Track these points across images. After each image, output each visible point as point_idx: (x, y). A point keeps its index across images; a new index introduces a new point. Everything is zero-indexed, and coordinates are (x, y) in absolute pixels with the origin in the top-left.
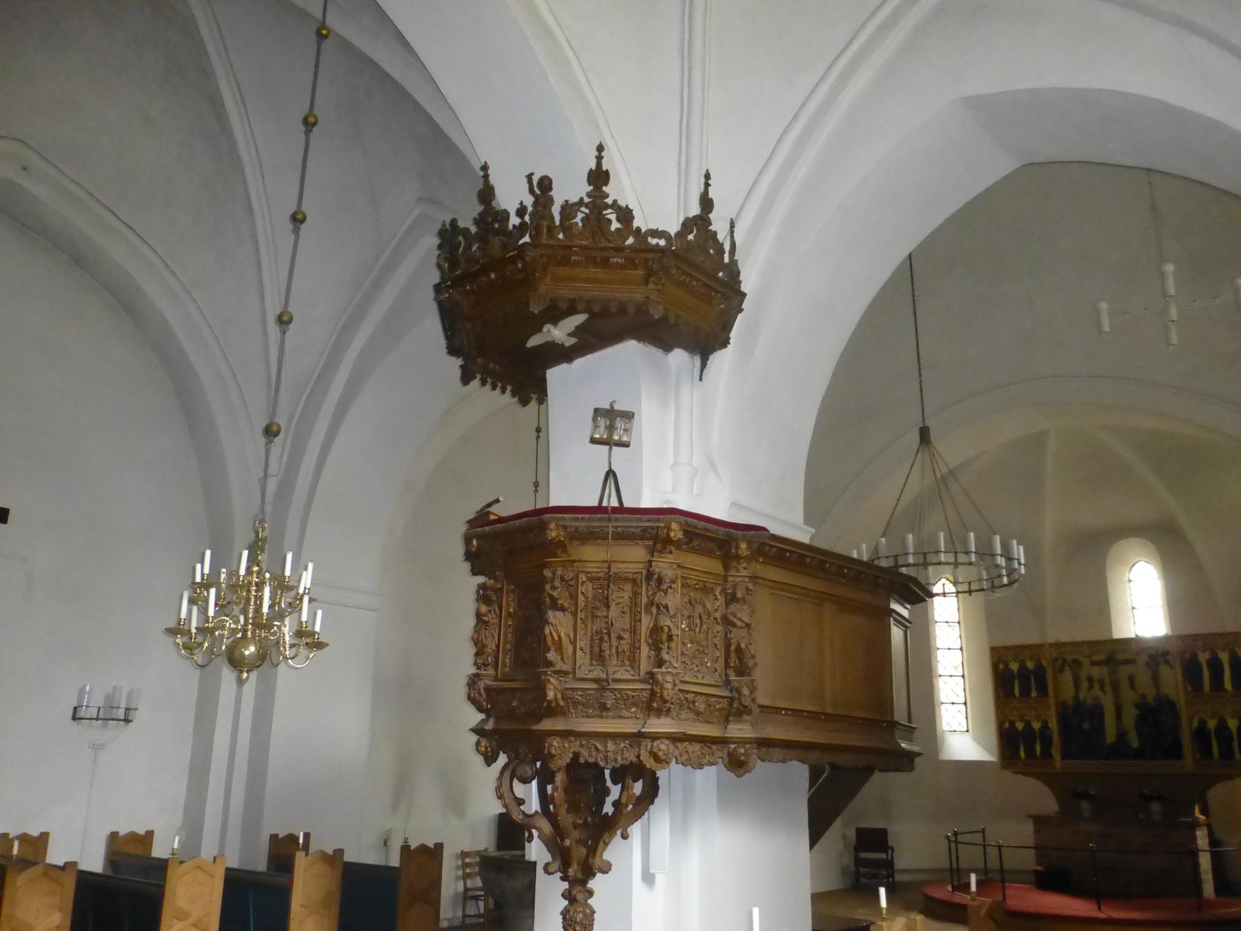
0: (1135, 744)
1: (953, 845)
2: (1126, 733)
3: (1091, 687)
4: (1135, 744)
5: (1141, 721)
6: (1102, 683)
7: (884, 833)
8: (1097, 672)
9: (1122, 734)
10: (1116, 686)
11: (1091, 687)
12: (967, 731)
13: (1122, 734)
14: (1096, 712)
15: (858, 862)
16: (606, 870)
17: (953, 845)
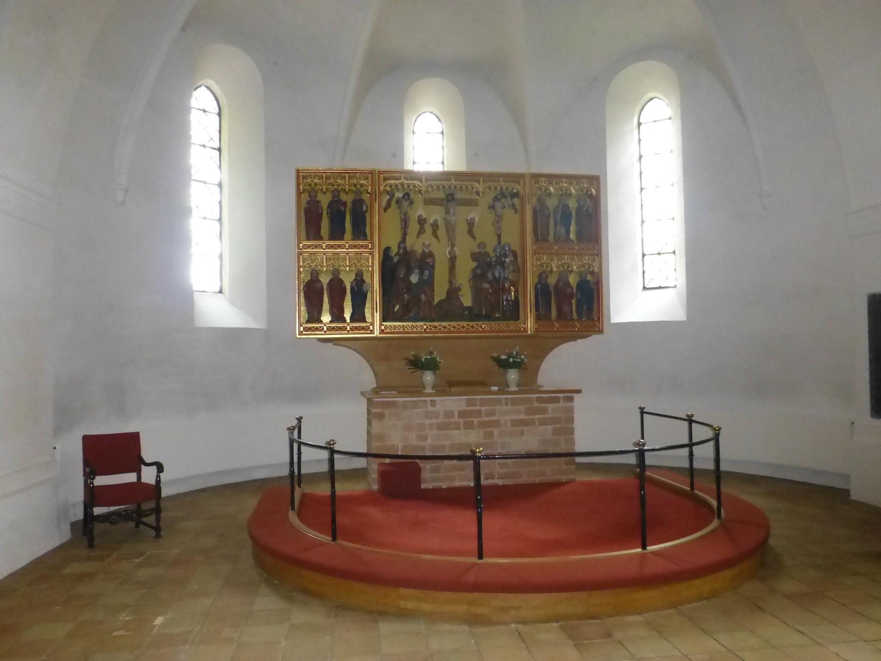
0: (467, 300)
1: (295, 446)
2: (459, 289)
3: (422, 231)
4: (467, 300)
5: (477, 277)
6: (435, 226)
7: (133, 439)
8: (435, 215)
9: (453, 292)
10: (450, 229)
11: (422, 231)
12: (221, 292)
13: (453, 292)
14: (426, 262)
15: (93, 496)
16: (315, 272)
17: (295, 446)
